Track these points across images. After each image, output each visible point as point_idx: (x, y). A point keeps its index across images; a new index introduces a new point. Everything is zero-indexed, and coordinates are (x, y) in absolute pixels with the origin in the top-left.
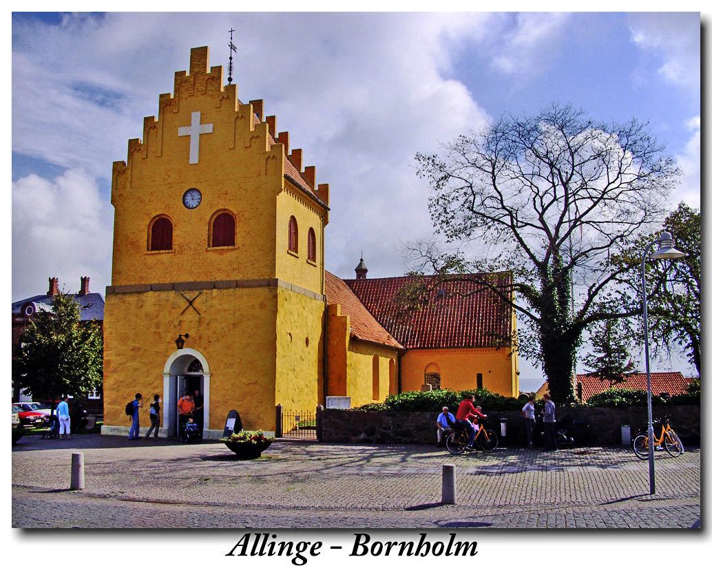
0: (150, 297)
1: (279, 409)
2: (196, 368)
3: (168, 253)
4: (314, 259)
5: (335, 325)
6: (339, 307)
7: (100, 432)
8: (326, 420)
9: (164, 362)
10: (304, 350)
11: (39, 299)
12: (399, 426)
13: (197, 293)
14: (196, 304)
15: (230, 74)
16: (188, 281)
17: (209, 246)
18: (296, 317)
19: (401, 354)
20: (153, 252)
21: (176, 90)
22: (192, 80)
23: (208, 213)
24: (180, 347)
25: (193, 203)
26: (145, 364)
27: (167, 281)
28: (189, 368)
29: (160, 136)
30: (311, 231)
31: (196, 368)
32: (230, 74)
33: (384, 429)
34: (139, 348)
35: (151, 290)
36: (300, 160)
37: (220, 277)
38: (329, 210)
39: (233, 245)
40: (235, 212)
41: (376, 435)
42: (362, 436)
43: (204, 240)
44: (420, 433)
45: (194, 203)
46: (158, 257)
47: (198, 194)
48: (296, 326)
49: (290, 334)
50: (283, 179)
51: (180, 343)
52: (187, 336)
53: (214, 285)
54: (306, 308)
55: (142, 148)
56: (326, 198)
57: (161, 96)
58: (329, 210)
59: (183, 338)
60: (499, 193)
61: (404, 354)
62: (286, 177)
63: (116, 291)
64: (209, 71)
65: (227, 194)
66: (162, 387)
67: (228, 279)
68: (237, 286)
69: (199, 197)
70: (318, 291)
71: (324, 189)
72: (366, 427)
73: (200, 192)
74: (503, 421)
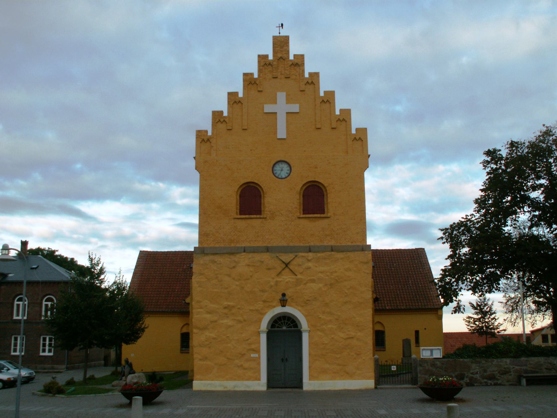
0: (243, 259)
2: (279, 324)
8: (421, 368)
9: (260, 321)
12: (485, 371)
16: (280, 245)
21: (260, 71)
23: (298, 183)
24: (283, 306)
26: (240, 321)
27: (260, 244)
31: (279, 324)
33: (472, 373)
34: (233, 307)
35: (244, 251)
37: (313, 242)
39: (323, 212)
41: (466, 379)
43: (296, 208)
44: (502, 376)
45: (284, 174)
47: (288, 168)
51: (283, 303)
53: (310, 250)
57: (229, 94)
63: (205, 252)
65: (316, 168)
66: (259, 343)
67: (321, 244)
68: (332, 251)
72: (456, 373)
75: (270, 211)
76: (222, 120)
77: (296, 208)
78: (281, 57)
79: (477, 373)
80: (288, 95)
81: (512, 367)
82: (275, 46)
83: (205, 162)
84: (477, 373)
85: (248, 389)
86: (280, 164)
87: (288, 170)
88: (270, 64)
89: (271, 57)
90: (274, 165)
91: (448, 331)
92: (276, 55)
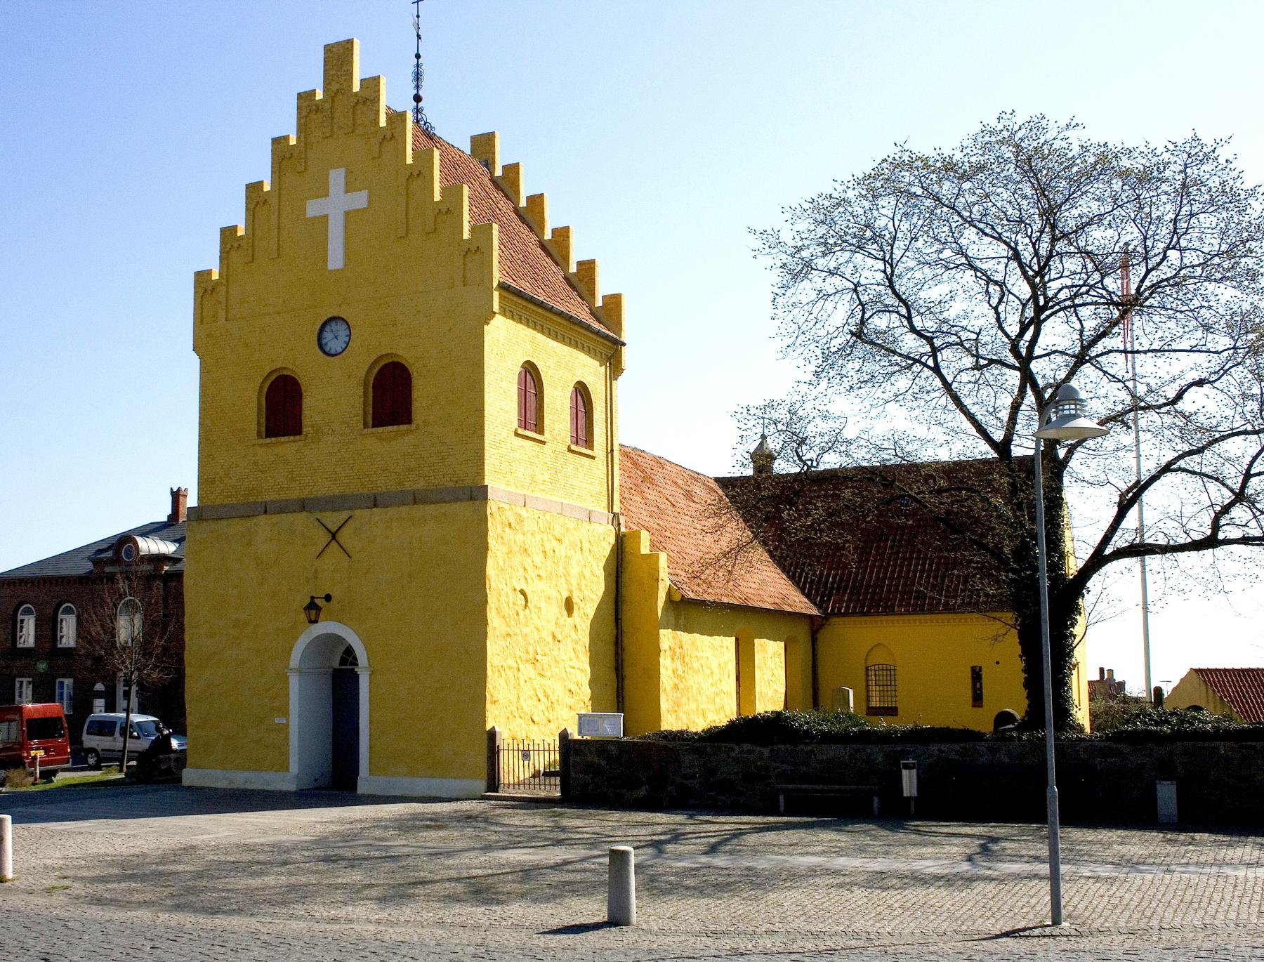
1: (492, 735)
3: (294, 441)
4: (589, 443)
5: (633, 571)
6: (645, 537)
7: (356, 789)
10: (561, 621)
11: (151, 530)
13: (344, 515)
14: (344, 537)
15: (418, 87)
17: (365, 426)
18: (538, 559)
19: (815, 626)
20: (268, 440)
22: (327, 106)
25: (334, 345)
28: (342, 658)
29: (274, 218)
30: (582, 391)
32: (418, 87)
36: (566, 250)
38: (624, 344)
40: (411, 361)
42: (642, 792)
43: (358, 415)
46: (279, 450)
47: (345, 326)
48: (539, 576)
49: (523, 592)
50: (496, 295)
51: (313, 610)
52: (328, 598)
54: (566, 541)
55: (243, 244)
56: (617, 325)
58: (624, 344)
59: (319, 602)
60: (904, 302)
61: (821, 626)
62: (503, 287)
64: (356, 87)
65: (395, 325)
69: (347, 331)
70: (601, 507)
71: (614, 302)
73: (343, 319)
74: (907, 767)
75: (312, 426)
76: (236, 245)
77: (358, 415)
78: (338, 90)
79: (693, 777)
80: (349, 173)
81: (774, 765)
82: (327, 67)
83: (208, 336)
84: (693, 777)
85: (269, 788)
86: (328, 328)
87: (330, 349)
88: (318, 108)
89: (319, 95)
90: (324, 326)
91: (718, 640)
92: (329, 87)
